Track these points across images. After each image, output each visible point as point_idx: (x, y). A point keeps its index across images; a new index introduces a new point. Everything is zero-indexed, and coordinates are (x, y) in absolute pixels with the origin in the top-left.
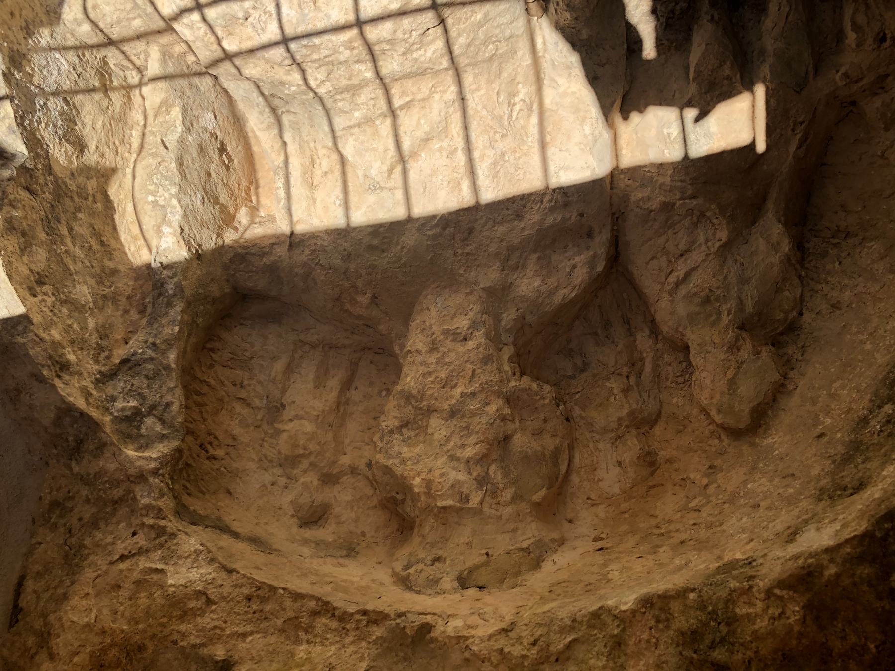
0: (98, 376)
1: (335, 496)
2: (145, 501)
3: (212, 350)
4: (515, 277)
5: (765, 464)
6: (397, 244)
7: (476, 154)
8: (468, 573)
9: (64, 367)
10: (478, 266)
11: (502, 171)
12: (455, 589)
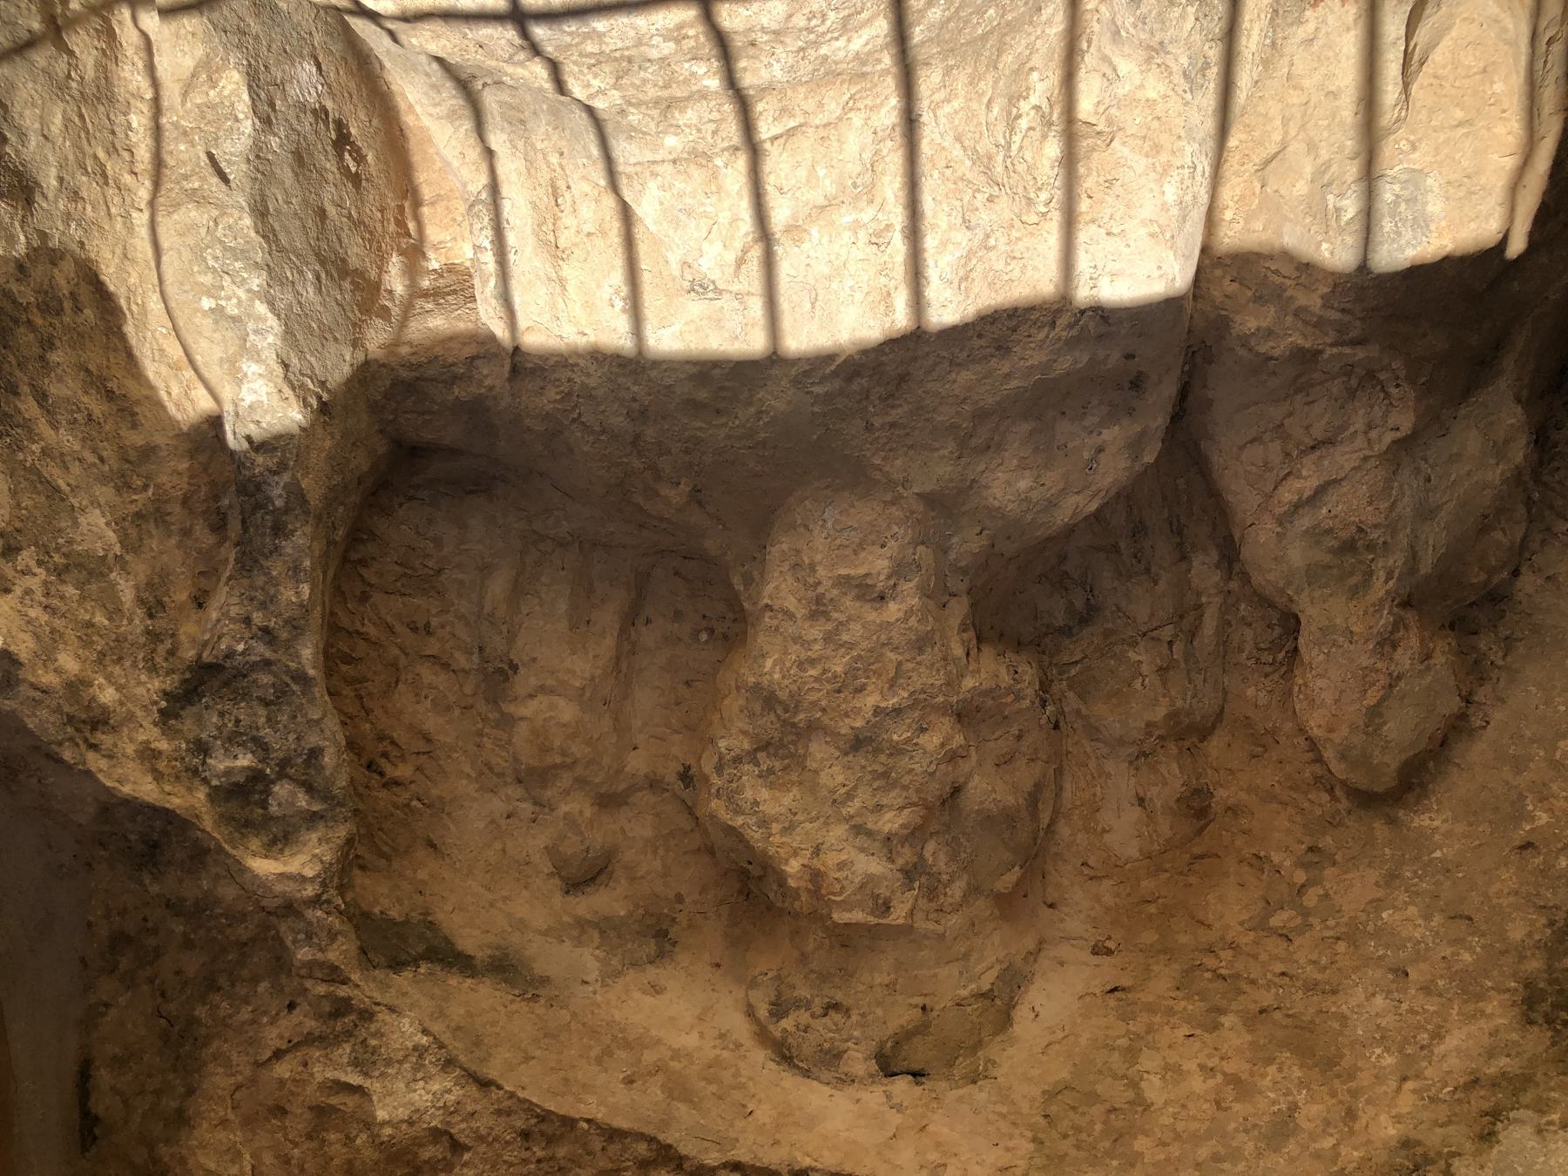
0: (163, 704)
1: (622, 828)
2: (304, 954)
3: (363, 562)
4: (981, 467)
5: (1415, 872)
6: (750, 404)
7: (930, 242)
8: (892, 1047)
9: (98, 721)
10: (911, 447)
11: (979, 268)
12: (871, 1076)
